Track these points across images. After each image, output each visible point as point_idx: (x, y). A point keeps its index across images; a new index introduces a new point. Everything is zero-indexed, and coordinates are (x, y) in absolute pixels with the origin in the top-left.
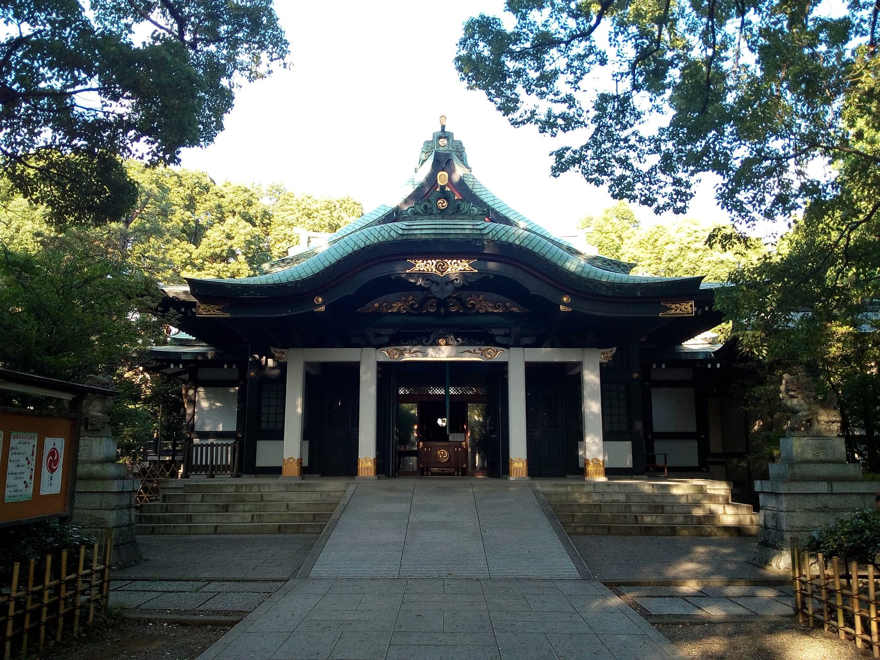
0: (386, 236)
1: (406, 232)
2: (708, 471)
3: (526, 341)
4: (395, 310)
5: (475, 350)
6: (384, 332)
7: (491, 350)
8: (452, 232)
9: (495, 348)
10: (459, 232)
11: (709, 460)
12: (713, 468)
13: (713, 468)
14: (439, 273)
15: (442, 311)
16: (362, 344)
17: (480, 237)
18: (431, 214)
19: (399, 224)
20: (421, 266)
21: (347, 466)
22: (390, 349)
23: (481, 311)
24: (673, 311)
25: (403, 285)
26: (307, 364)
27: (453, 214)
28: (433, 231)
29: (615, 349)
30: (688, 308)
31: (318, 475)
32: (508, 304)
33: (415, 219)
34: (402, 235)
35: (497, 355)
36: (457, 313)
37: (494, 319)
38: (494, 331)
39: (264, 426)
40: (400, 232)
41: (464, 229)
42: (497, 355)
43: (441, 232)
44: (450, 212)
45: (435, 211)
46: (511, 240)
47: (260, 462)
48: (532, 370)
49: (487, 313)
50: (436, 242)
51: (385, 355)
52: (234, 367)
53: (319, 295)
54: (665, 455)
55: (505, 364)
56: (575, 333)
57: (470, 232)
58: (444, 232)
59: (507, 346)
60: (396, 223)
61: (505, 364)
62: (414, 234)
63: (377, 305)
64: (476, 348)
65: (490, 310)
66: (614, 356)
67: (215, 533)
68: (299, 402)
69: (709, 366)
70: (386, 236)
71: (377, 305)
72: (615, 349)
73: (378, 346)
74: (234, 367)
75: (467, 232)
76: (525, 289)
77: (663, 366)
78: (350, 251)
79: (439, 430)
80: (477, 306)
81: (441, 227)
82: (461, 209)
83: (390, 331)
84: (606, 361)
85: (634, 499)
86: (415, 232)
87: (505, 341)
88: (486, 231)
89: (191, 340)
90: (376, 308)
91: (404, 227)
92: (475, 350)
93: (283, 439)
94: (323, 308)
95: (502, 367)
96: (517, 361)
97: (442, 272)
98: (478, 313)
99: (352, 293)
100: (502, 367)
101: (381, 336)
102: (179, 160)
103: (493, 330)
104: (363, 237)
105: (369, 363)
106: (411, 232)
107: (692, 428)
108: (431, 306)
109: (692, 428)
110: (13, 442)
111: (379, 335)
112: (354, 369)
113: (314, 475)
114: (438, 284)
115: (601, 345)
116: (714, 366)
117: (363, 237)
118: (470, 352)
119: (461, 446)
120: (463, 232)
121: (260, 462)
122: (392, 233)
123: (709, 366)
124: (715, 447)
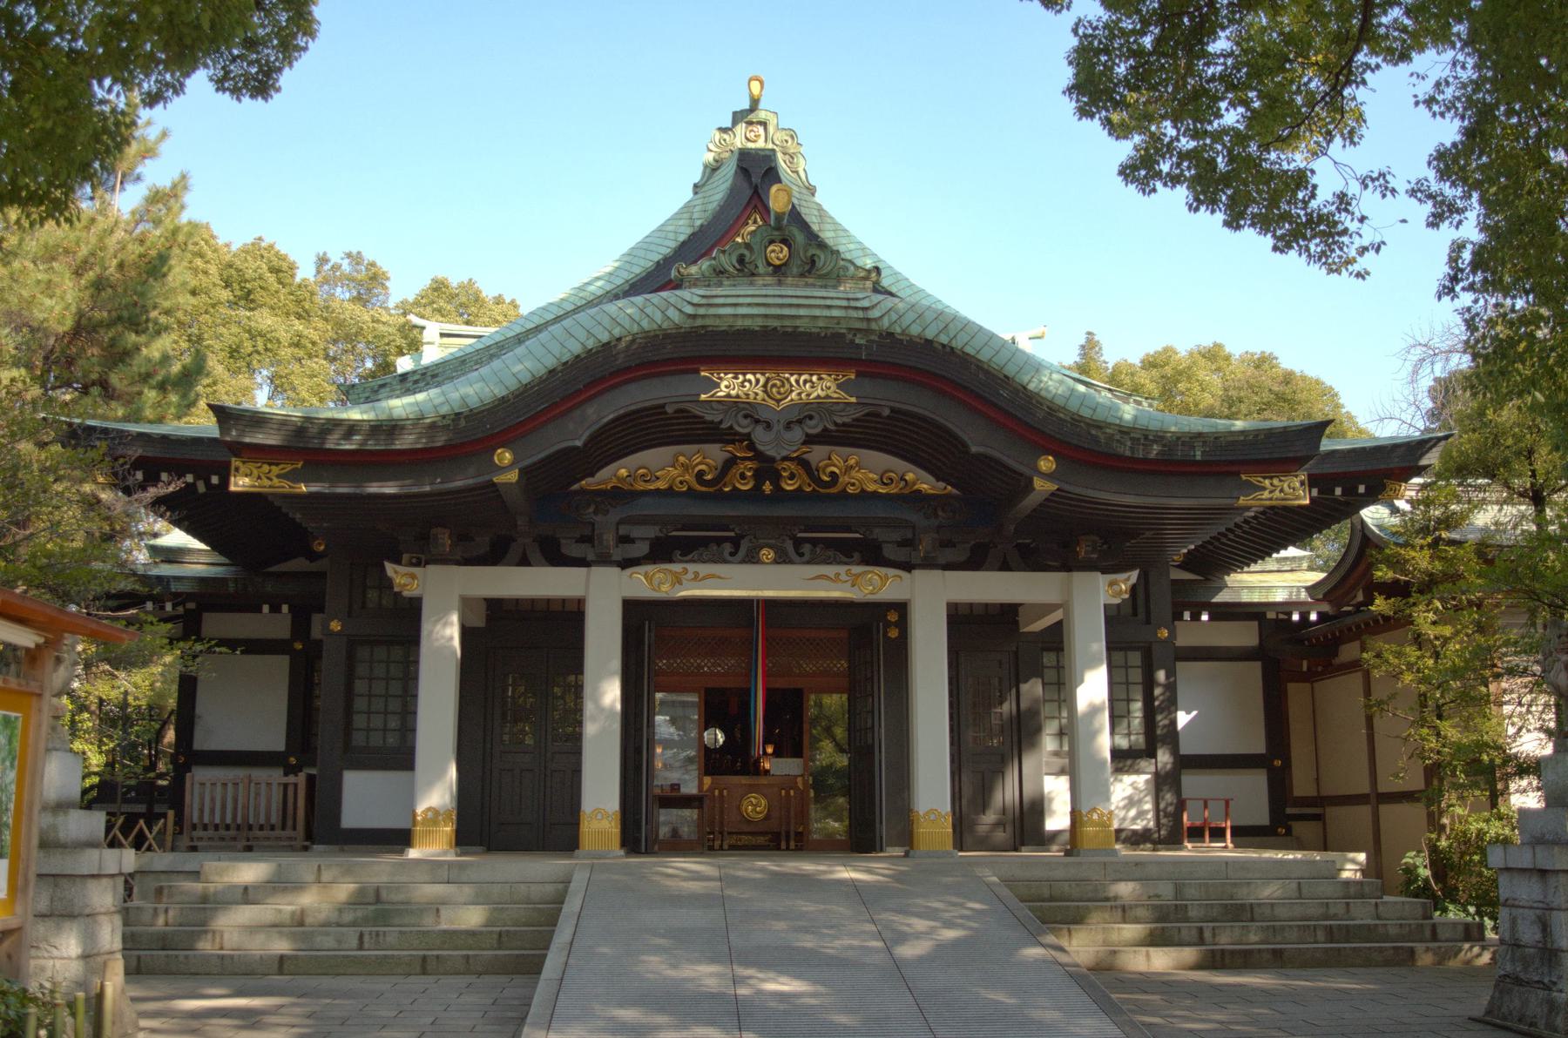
0: (658, 317)
1: (702, 311)
2: (1289, 832)
3: (949, 555)
4: (661, 485)
5: (838, 574)
7: (875, 574)
8: (802, 312)
9: (883, 571)
10: (817, 312)
11: (1289, 811)
13: (1299, 828)
14: (771, 403)
15: (767, 487)
17: (864, 325)
18: (753, 275)
19: (685, 294)
20: (729, 385)
21: (556, 830)
22: (650, 568)
23: (850, 490)
24: (1266, 494)
25: (690, 427)
27: (802, 275)
28: (762, 311)
29: (1134, 576)
30: (1295, 491)
31: (480, 849)
32: (910, 477)
33: (720, 284)
34: (694, 317)
38: (878, 534)
39: (358, 739)
40: (689, 310)
41: (829, 307)
43: (778, 311)
44: (795, 270)
45: (761, 269)
46: (929, 334)
47: (354, 815)
48: (636, 613)
50: (767, 333)
52: (285, 608)
54: (1227, 802)
55: (902, 608)
56: (1058, 542)
58: (786, 311)
59: (908, 567)
60: (678, 292)
61: (902, 608)
62: (719, 316)
64: (842, 569)
65: (871, 487)
67: (281, 973)
68: (588, 804)
69: (1296, 617)
70: (658, 317)
71: (623, 472)
72: (1134, 576)
73: (625, 564)
74: (285, 608)
75: (835, 313)
76: (966, 446)
77: (1205, 617)
78: (576, 349)
79: (786, 743)
80: (843, 480)
81: (780, 301)
82: (819, 264)
83: (652, 532)
84: (1117, 601)
85: (1191, 892)
86: (722, 311)
87: (901, 554)
88: (875, 314)
90: (621, 480)
91: (696, 300)
92: (838, 574)
96: (930, 598)
97: (778, 401)
99: (579, 443)
102: (1197, 210)
103: (877, 531)
104: (606, 322)
105: (603, 595)
106: (712, 311)
107: (1258, 746)
109: (1258, 746)
111: (625, 540)
113: (474, 848)
114: (768, 426)
115: (1109, 565)
117: (606, 322)
119: (796, 788)
120: (826, 313)
121: (354, 815)
122: (672, 313)
123: (1296, 617)
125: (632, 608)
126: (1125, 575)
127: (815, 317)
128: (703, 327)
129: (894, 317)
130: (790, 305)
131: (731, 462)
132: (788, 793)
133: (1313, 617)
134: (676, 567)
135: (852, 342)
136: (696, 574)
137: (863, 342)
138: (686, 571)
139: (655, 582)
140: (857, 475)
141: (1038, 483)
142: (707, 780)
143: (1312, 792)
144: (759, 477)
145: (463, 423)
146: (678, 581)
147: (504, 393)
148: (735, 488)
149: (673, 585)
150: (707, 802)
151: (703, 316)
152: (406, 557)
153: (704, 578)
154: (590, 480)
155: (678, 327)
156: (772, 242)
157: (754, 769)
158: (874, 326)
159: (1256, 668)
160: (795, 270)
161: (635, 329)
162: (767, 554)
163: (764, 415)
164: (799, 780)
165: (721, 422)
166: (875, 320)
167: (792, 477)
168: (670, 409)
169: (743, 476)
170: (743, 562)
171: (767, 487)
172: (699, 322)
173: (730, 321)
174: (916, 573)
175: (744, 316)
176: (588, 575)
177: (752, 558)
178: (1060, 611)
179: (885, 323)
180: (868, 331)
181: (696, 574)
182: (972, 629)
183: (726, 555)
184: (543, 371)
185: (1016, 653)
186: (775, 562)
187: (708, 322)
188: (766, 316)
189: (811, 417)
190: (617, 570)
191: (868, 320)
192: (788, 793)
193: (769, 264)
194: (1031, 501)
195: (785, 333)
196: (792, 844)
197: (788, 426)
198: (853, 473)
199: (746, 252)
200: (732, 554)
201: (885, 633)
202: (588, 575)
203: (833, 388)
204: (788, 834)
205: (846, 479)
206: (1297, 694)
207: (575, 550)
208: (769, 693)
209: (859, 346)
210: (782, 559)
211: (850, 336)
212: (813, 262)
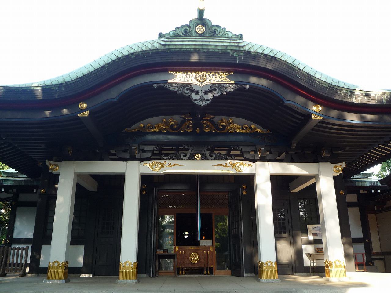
2: (373, 264)
6: (146, 148)
8: (211, 43)
10: (217, 44)
12: (376, 263)
13: (376, 263)
15: (198, 131)
16: (128, 157)
17: (238, 49)
22: (152, 162)
26: (79, 176)
28: (194, 43)
32: (253, 126)
35: (244, 168)
36: (210, 133)
37: (241, 138)
42: (244, 168)
49: (235, 133)
51: (149, 168)
53: (84, 101)
56: (312, 150)
57: (228, 44)
62: (176, 45)
63: (142, 125)
65: (238, 131)
66: (344, 170)
69: (373, 191)
72: (344, 164)
73: (141, 160)
82: (217, 33)
89: (15, 173)
90: (141, 128)
93: (51, 244)
94: (86, 114)
95: (249, 180)
98: (228, 133)
100: (249, 180)
101: (144, 151)
105: (133, 172)
108: (188, 127)
110: (277, 243)
112: (120, 179)
114: (197, 93)
115: (333, 160)
116: (376, 191)
118: (222, 165)
119: (210, 251)
123: (373, 191)
124: (376, 247)
125: (145, 179)
126: (340, 164)
127: (217, 46)
128: (169, 49)
129: (250, 46)
130: (206, 41)
131: (184, 121)
132: (207, 253)
133: (379, 191)
134: (162, 161)
135: (233, 56)
136: (170, 164)
137: (237, 56)
138: (165, 162)
139: (154, 167)
140: (232, 126)
141: (314, 116)
142: (177, 248)
143: (379, 251)
144: (195, 127)
145: (63, 89)
146: (162, 166)
147: (82, 75)
148: (185, 131)
149: (160, 168)
150: (177, 256)
151: (169, 45)
152: (55, 158)
153: (173, 165)
154: (129, 129)
155: (158, 49)
156: (198, 25)
157: (197, 244)
158: (242, 49)
159: (357, 209)
160: (208, 35)
161: (140, 50)
162: (198, 156)
163: (195, 88)
164: (211, 248)
165: (177, 91)
166: (242, 47)
167: (207, 127)
168: (155, 86)
169: (188, 127)
170: (188, 159)
171: (198, 131)
172: (167, 47)
173: (180, 47)
174: (257, 163)
175: (186, 45)
176: (127, 163)
177: (192, 158)
178: (314, 179)
179: (246, 48)
180: (239, 51)
181: (170, 164)
182: (280, 184)
183: (182, 156)
184: (99, 67)
185: (289, 200)
186: (201, 159)
187: (171, 47)
188: (195, 45)
189: (215, 90)
190: (138, 162)
191: (239, 47)
192: (207, 253)
193: (197, 33)
194: (309, 126)
195: (204, 52)
196: (209, 272)
197: (206, 93)
198: (231, 125)
199: (188, 28)
200: (184, 156)
201: (242, 193)
202: (127, 163)
203: (225, 77)
204: (207, 268)
205: (229, 128)
206: (371, 218)
207: (122, 155)
208: (201, 214)
209: (236, 58)
210: (204, 158)
211: (232, 53)
212: (215, 32)
